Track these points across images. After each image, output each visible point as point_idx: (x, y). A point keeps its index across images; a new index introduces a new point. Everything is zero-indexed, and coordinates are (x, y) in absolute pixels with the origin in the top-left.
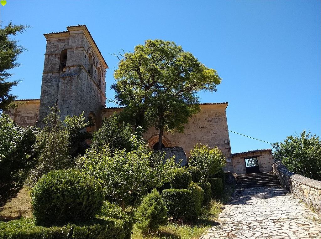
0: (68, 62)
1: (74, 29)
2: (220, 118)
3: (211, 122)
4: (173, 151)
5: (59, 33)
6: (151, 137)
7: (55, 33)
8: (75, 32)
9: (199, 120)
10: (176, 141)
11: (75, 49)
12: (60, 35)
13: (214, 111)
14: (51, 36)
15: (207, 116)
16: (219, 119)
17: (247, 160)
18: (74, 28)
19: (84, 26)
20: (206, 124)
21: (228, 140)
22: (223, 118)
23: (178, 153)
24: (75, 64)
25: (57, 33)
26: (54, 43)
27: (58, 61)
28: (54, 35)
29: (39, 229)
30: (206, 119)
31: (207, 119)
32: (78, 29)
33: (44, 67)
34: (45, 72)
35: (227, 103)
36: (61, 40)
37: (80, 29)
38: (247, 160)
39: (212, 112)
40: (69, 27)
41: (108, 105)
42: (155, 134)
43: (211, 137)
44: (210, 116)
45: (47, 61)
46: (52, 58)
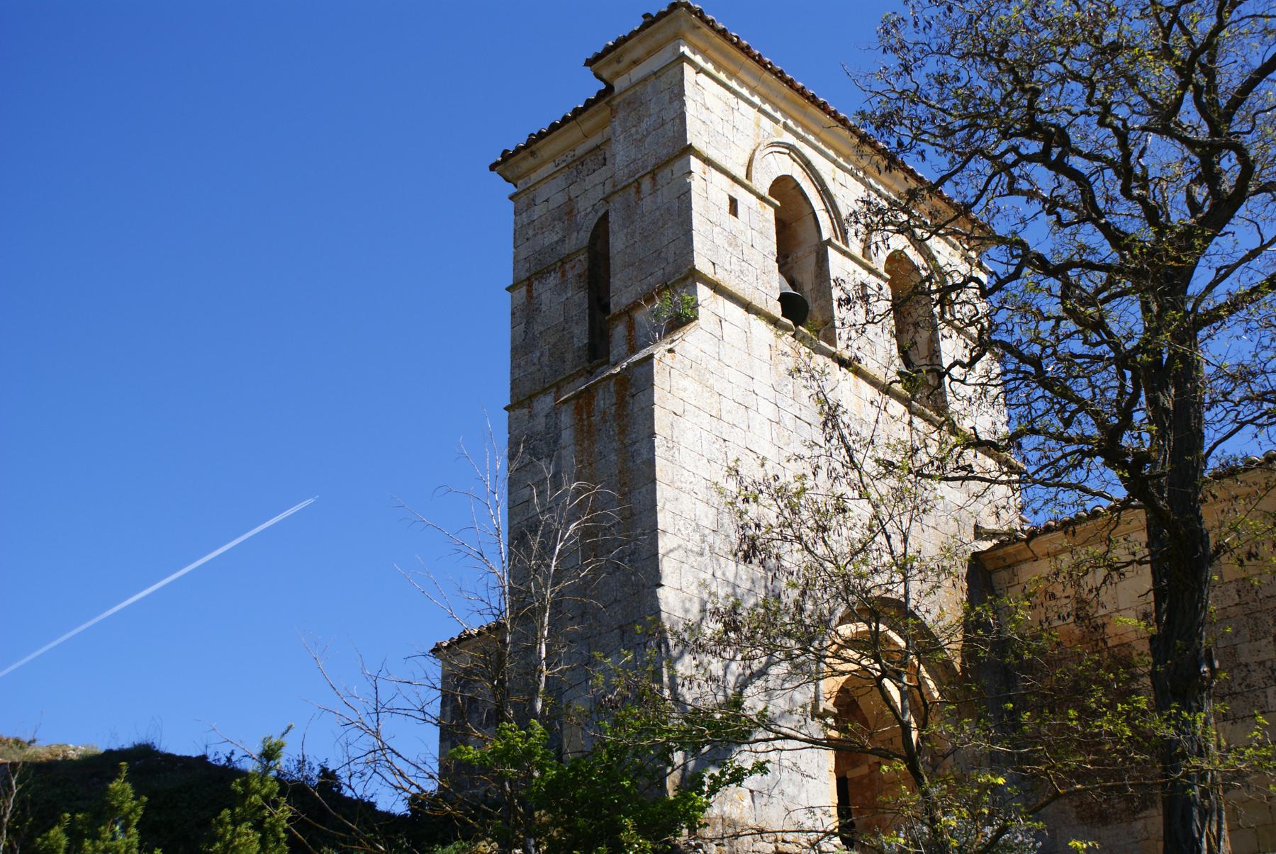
0: (616, 282)
1: (627, 60)
5: (565, 120)
7: (541, 136)
8: (638, 72)
11: (646, 184)
12: (572, 134)
14: (531, 161)
17: (1114, 366)
19: (674, 7)
25: (554, 127)
26: (552, 194)
27: (579, 298)
28: (548, 149)
29: (1160, 805)
32: (651, 43)
33: (513, 368)
34: (520, 401)
36: (581, 160)
37: (660, 37)
38: (1114, 366)
40: (598, 57)
41: (1205, 475)
45: (525, 315)
46: (546, 291)
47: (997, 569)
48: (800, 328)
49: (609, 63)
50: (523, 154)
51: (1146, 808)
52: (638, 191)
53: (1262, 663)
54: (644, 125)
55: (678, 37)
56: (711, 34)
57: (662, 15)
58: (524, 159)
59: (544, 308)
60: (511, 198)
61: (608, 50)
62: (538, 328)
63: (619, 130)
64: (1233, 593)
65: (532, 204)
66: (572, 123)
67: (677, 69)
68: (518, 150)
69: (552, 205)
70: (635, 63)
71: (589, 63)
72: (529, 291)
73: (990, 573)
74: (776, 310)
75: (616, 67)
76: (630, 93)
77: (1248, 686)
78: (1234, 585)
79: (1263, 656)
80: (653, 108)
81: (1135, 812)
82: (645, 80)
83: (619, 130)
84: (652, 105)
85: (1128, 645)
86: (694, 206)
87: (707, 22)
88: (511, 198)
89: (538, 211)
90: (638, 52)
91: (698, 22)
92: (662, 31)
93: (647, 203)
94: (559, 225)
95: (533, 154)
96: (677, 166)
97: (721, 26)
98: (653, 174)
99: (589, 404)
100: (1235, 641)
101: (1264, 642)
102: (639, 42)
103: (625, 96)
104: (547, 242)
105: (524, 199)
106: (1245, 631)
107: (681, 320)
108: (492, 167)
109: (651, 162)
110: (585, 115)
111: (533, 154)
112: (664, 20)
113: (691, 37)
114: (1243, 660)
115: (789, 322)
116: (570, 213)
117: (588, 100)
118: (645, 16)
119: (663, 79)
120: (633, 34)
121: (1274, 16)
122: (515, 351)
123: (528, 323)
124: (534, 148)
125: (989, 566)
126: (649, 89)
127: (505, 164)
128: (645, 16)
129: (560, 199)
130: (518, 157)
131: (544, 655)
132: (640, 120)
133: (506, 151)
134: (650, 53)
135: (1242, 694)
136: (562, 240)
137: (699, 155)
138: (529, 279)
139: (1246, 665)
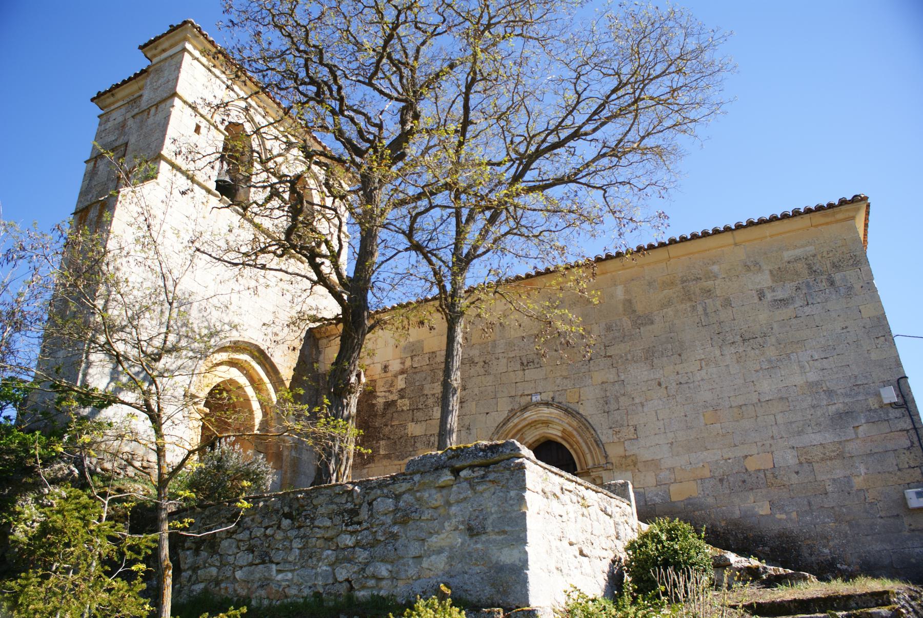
1: (160, 48)
2: (837, 277)
3: (791, 307)
4: (463, 474)
6: (508, 420)
7: (117, 86)
9: (727, 303)
10: (622, 425)
11: (153, 110)
13: (798, 252)
14: (112, 99)
15: (764, 280)
16: (832, 283)
18: (160, 44)
19: (185, 22)
20: (763, 317)
21: (901, 384)
22: (851, 275)
23: (493, 482)
24: (482, 258)
25: (124, 82)
28: (121, 93)
30: (761, 295)
31: (769, 296)
32: (172, 41)
33: (78, 202)
35: (857, 199)
37: (177, 38)
39: (788, 255)
40: (146, 45)
42: (524, 401)
43: (799, 380)
44: (779, 275)
47: (321, 338)
48: (224, 197)
49: (151, 49)
50: (108, 94)
51: (370, 463)
52: (148, 114)
53: (433, 395)
54: (160, 82)
55: (185, 39)
56: (205, 42)
57: (179, 26)
58: (108, 97)
59: (99, 173)
60: (99, 117)
61: (151, 42)
62: (94, 183)
63: (149, 83)
64: (427, 359)
65: (108, 120)
66: (134, 81)
67: (181, 55)
68: (106, 92)
69: (116, 122)
70: (164, 51)
71: (141, 48)
72: (95, 164)
73: (318, 339)
74: (212, 186)
75: (154, 52)
76: (158, 65)
77: (426, 405)
78: (427, 355)
79: (435, 391)
80: (166, 73)
81: (364, 465)
82: (166, 59)
83: (149, 83)
84: (166, 72)
85: (375, 381)
86: (171, 122)
87: (203, 35)
88: (99, 117)
89: (110, 124)
90: (166, 45)
91: (198, 34)
92: (178, 35)
93: (150, 121)
94: (117, 132)
95: (113, 95)
96: (169, 102)
97: (211, 39)
98: (157, 105)
99: (86, 215)
100: (424, 383)
101: (436, 384)
102: (167, 40)
103: (155, 67)
104: (109, 140)
105: (104, 118)
106: (429, 379)
107: (149, 176)
108: (92, 100)
109: (159, 99)
110: (140, 77)
111: (113, 95)
112: (179, 29)
113: (193, 41)
114: (425, 392)
115: (218, 193)
116: (123, 127)
117: (142, 70)
118: (170, 26)
119: (174, 60)
120: (163, 35)
121: (376, 2)
122: (81, 193)
123: (90, 180)
124: (114, 92)
125: (318, 336)
126: (167, 64)
127: (98, 98)
128: (171, 26)
129: (120, 119)
130: (106, 96)
131: (845, 613)
132: (158, 79)
133: (99, 92)
134: (172, 46)
135: (422, 409)
136: (116, 140)
137: (180, 98)
138: (96, 158)
139: (427, 395)
